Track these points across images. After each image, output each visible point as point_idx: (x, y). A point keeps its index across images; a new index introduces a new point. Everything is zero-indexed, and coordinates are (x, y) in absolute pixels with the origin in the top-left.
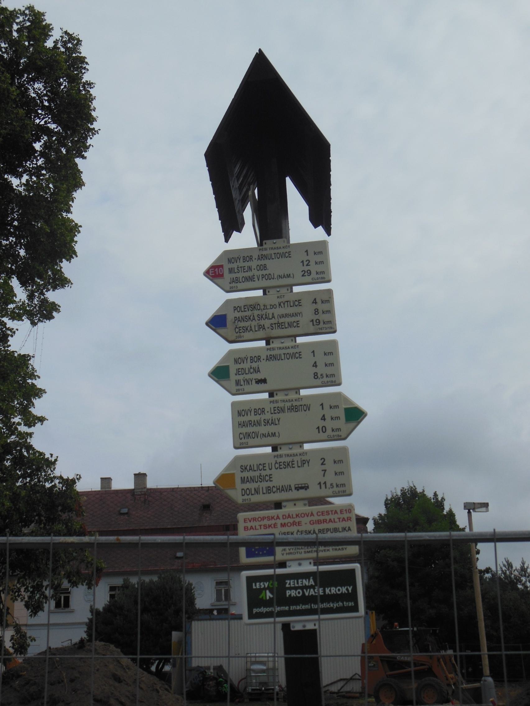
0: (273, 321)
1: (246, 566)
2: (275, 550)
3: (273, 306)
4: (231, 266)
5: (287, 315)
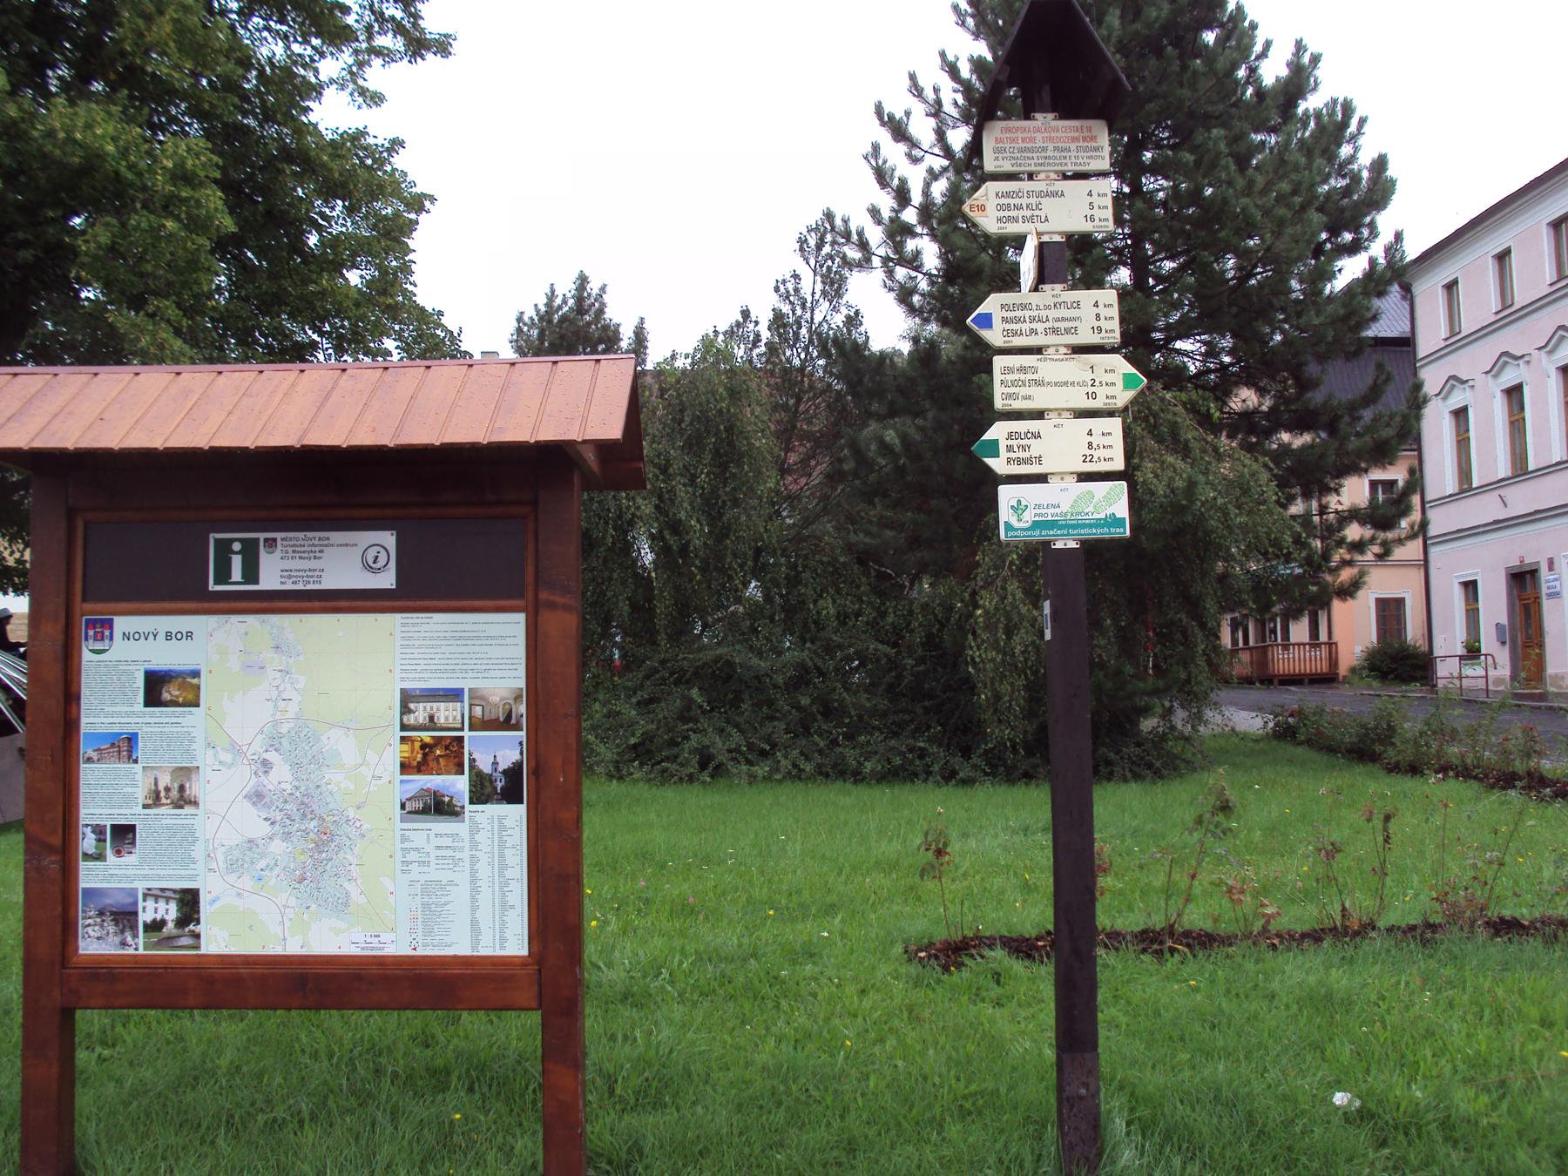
0: (1048, 325)
1: (858, 777)
2: (228, 962)
3: (1047, 307)
4: (1010, 442)
5: (1063, 319)
